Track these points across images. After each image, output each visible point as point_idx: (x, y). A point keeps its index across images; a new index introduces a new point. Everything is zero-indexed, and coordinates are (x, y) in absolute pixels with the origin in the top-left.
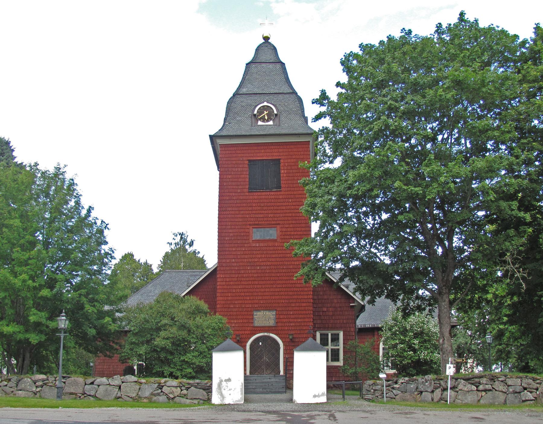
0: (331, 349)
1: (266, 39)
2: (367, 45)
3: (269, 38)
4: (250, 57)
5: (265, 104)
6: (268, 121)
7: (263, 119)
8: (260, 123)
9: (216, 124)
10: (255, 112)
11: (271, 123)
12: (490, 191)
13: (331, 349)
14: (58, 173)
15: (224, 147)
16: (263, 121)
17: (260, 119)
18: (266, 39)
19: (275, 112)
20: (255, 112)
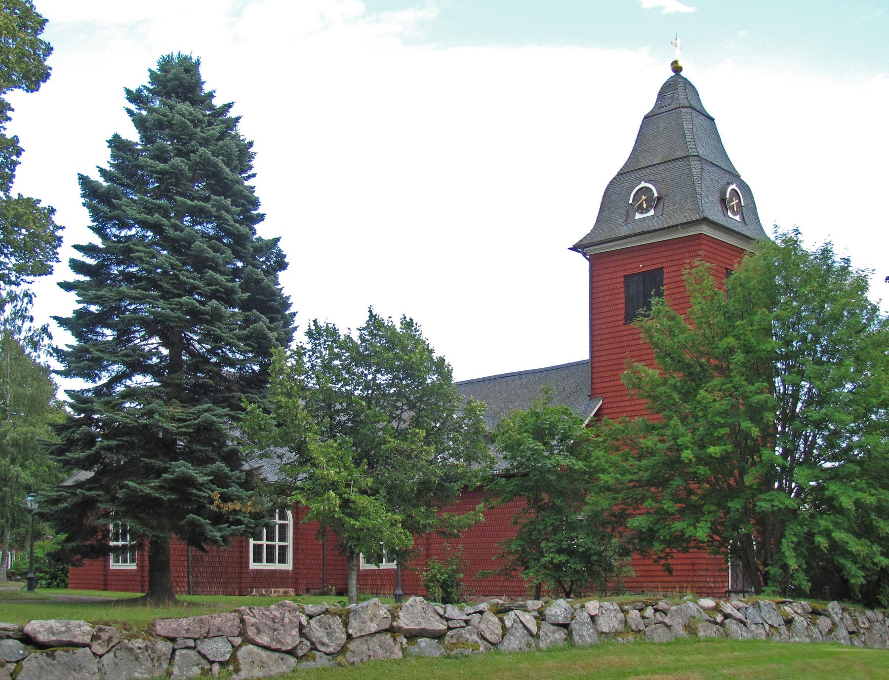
0: (267, 545)
1: (676, 68)
2: (61, 362)
3: (681, 69)
4: (648, 104)
5: (643, 184)
6: (647, 211)
7: (640, 209)
8: (638, 216)
9: (584, 222)
10: (631, 201)
11: (652, 213)
12: (102, 452)
13: (267, 545)
14: (374, 323)
15: (600, 253)
16: (642, 213)
17: (637, 211)
18: (676, 68)
19: (656, 195)
20: (631, 201)
